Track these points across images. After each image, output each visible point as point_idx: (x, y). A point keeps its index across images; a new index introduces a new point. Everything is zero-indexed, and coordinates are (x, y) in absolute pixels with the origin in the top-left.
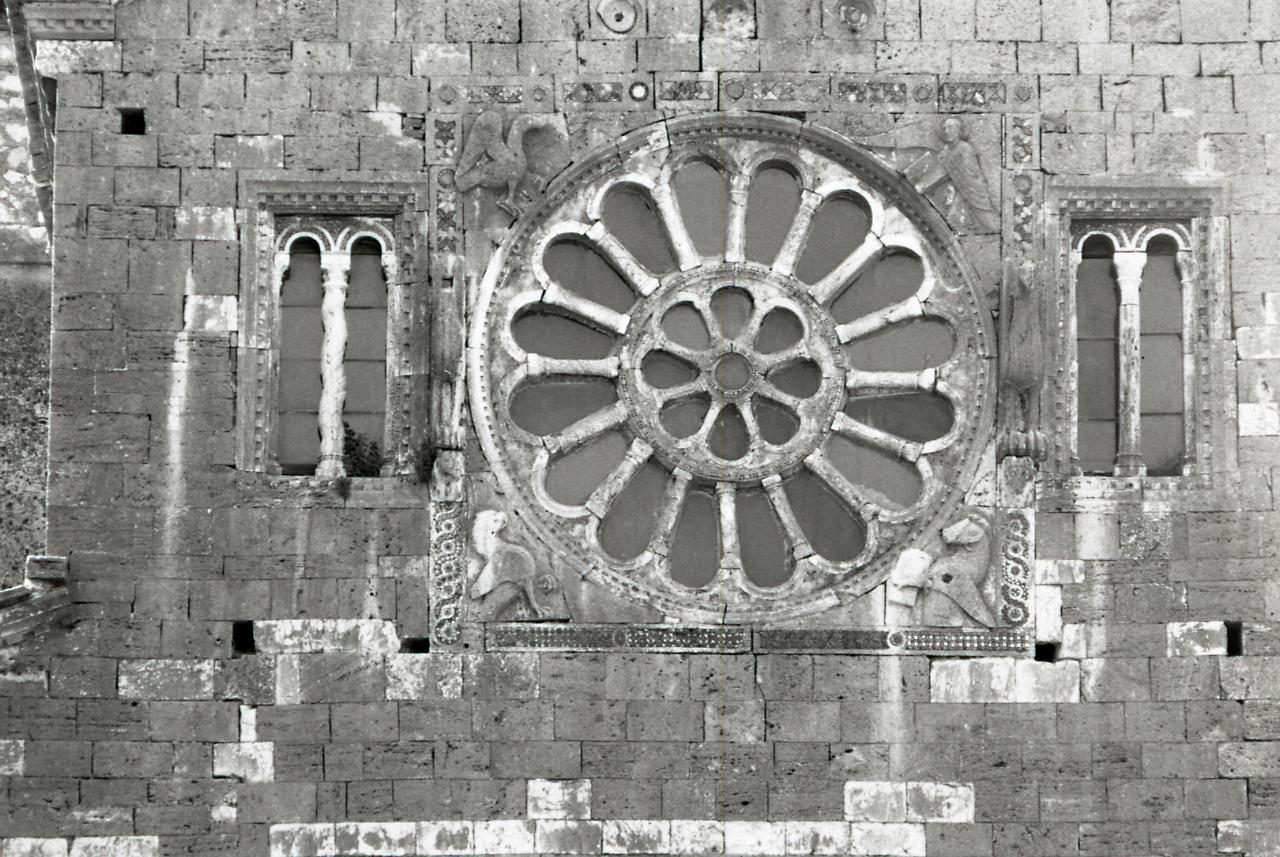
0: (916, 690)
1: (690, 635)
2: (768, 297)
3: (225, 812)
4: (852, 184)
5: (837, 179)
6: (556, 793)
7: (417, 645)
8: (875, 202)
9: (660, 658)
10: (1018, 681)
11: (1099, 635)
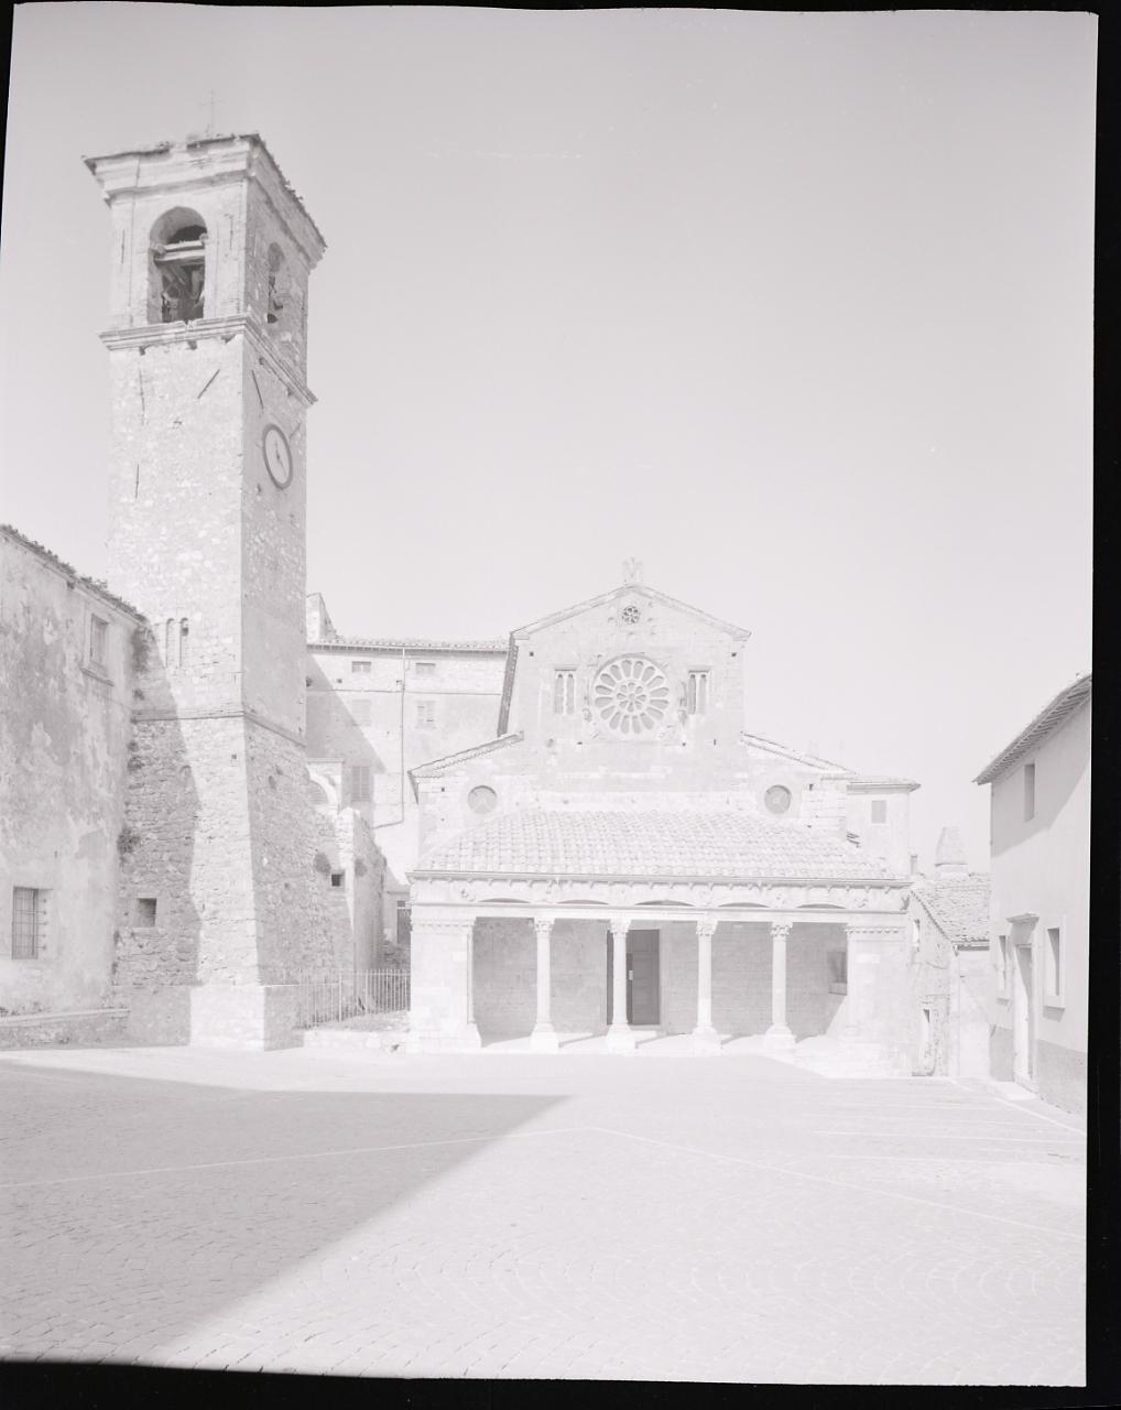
1: (625, 742)
2: (638, 684)
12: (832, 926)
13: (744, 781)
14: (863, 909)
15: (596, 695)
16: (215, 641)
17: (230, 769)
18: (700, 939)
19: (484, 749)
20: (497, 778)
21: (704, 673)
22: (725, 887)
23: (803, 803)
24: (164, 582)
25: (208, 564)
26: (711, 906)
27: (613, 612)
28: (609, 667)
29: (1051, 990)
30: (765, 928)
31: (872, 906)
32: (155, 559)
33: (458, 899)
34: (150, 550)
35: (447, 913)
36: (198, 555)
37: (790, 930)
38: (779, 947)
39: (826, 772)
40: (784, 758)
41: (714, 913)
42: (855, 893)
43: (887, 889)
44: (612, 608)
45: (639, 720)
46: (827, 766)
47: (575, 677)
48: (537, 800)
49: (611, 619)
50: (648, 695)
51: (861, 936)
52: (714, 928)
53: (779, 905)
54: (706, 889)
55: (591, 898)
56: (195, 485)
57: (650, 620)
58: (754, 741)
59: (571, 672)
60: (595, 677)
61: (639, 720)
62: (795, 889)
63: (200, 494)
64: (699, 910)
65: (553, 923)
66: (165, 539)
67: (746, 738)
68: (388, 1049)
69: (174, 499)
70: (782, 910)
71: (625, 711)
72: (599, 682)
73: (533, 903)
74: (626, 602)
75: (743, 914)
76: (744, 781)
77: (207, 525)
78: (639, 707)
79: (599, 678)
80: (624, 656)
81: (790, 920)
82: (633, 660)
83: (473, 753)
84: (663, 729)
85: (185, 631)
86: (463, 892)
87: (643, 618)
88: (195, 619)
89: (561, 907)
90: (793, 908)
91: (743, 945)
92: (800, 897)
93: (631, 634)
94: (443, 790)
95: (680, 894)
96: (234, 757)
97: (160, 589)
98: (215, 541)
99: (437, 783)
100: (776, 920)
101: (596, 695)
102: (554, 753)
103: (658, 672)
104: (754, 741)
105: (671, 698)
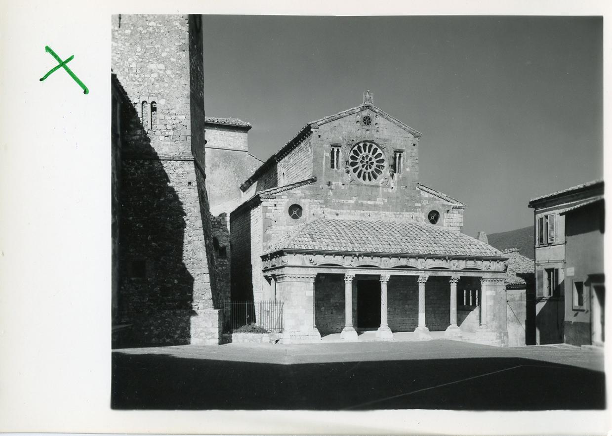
0: (382, 190)
1: (365, 185)
2: (370, 156)
3: (329, 198)
4: (377, 147)
5: (375, 147)
6: (355, 198)
7: (343, 185)
8: (378, 149)
9: (363, 187)
10: (390, 190)
11: (396, 187)
12: (477, 277)
13: (419, 207)
14: (489, 270)
15: (351, 161)
16: (173, 117)
17: (188, 190)
18: (420, 284)
19: (297, 185)
20: (303, 200)
21: (401, 151)
22: (431, 260)
23: (444, 219)
24: (140, 80)
25: (169, 72)
26: (425, 269)
27: (359, 118)
28: (356, 147)
29: (576, 303)
30: (449, 278)
31: (492, 269)
32: (134, 65)
33: (309, 264)
34: (130, 60)
35: (303, 271)
36: (162, 66)
37: (458, 280)
38: (454, 288)
39: (454, 205)
40: (437, 198)
41: (427, 272)
42: (486, 263)
43: (498, 261)
44: (358, 116)
45: (371, 174)
46: (455, 202)
47: (340, 150)
48: (323, 213)
49: (358, 122)
50: (375, 162)
51: (488, 283)
52: (427, 279)
53: (454, 268)
54: (423, 260)
55: (372, 264)
56: (158, 25)
57: (376, 124)
58: (424, 188)
59: (339, 148)
60: (350, 152)
61: (371, 174)
62: (461, 261)
63: (162, 31)
64: (421, 270)
65: (459, 278)
66: (140, 54)
67: (420, 187)
68: (274, 342)
69: (145, 31)
70: (455, 270)
71: (364, 169)
72: (352, 154)
73: (345, 266)
74: (365, 113)
75: (466, 273)
76: (419, 207)
77: (168, 50)
78: (370, 168)
79: (352, 151)
80: (364, 141)
81: (459, 275)
82: (368, 144)
83: (291, 187)
84: (383, 180)
85: (154, 109)
86: (311, 260)
87: (373, 123)
88: (161, 103)
89: (357, 268)
90: (460, 270)
91: (403, 287)
92: (462, 264)
93: (367, 130)
94: (275, 205)
95: (412, 262)
96: (190, 183)
97: (136, 83)
98: (172, 59)
99: (271, 202)
100: (453, 275)
101: (351, 161)
102: (331, 189)
103: (379, 151)
104: (424, 188)
105: (385, 164)
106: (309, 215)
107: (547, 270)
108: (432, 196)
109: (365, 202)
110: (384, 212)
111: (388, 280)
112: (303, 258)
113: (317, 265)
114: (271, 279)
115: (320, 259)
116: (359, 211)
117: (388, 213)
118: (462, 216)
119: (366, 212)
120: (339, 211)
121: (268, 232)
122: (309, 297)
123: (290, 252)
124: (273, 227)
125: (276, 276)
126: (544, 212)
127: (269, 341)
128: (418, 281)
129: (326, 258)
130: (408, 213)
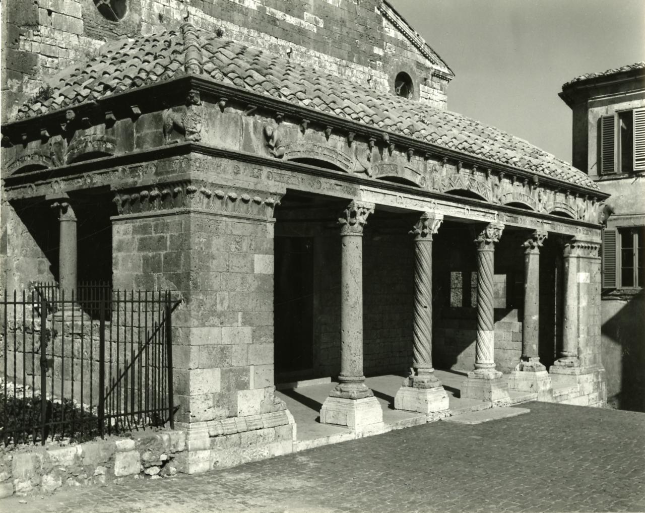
13: (380, 58)
35: (245, 177)
46: (438, 61)
104: (390, 13)
106: (150, 15)
107: (621, 230)
108: (401, 37)
109: (279, 15)
110: (318, 54)
111: (436, 232)
112: (247, 124)
113: (284, 159)
114: (65, 210)
115: (297, 141)
116: (267, 37)
117: (326, 57)
118: (445, 98)
119: (282, 42)
120: (224, 22)
121: (25, 46)
122: (262, 277)
123: (213, 94)
124: (43, 30)
125: (113, 194)
126: (617, 102)
127: (138, 467)
128: (481, 239)
129: (309, 138)
130: (361, 68)
